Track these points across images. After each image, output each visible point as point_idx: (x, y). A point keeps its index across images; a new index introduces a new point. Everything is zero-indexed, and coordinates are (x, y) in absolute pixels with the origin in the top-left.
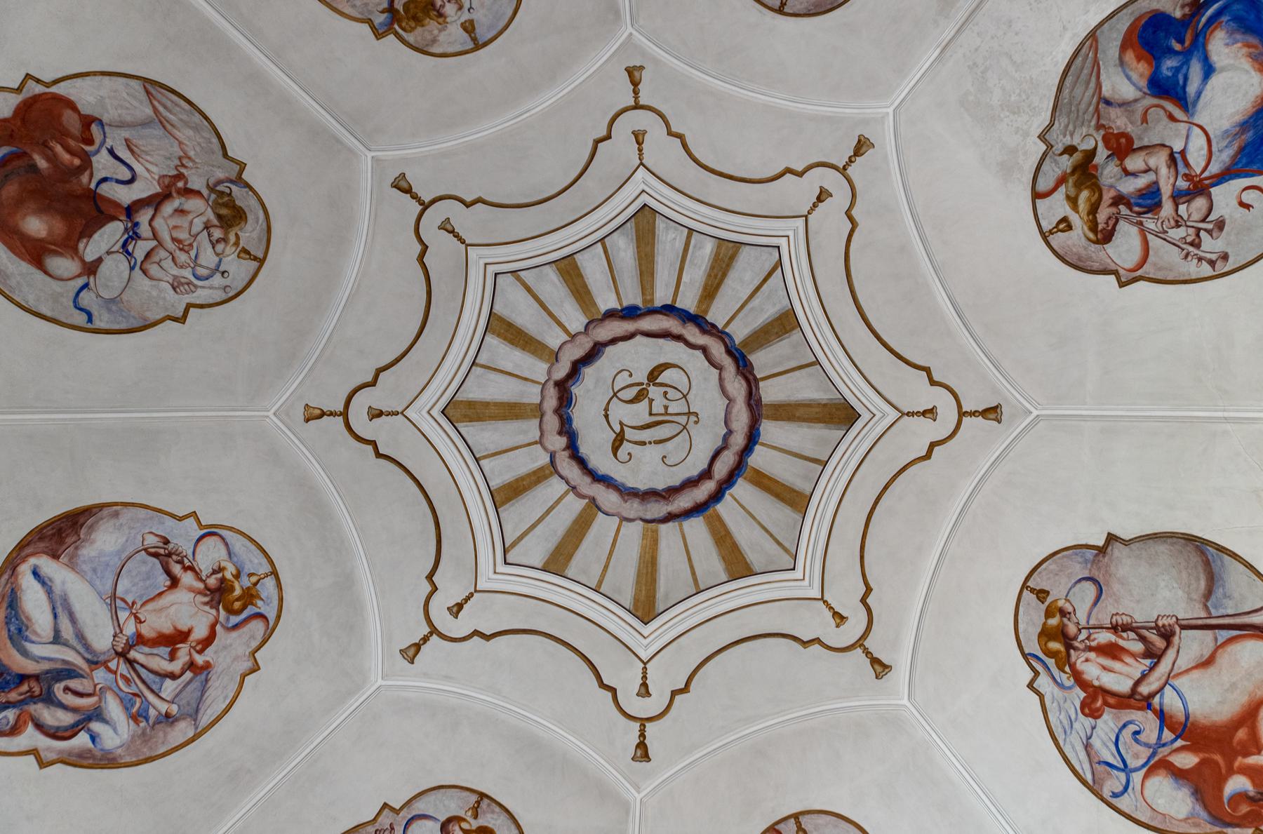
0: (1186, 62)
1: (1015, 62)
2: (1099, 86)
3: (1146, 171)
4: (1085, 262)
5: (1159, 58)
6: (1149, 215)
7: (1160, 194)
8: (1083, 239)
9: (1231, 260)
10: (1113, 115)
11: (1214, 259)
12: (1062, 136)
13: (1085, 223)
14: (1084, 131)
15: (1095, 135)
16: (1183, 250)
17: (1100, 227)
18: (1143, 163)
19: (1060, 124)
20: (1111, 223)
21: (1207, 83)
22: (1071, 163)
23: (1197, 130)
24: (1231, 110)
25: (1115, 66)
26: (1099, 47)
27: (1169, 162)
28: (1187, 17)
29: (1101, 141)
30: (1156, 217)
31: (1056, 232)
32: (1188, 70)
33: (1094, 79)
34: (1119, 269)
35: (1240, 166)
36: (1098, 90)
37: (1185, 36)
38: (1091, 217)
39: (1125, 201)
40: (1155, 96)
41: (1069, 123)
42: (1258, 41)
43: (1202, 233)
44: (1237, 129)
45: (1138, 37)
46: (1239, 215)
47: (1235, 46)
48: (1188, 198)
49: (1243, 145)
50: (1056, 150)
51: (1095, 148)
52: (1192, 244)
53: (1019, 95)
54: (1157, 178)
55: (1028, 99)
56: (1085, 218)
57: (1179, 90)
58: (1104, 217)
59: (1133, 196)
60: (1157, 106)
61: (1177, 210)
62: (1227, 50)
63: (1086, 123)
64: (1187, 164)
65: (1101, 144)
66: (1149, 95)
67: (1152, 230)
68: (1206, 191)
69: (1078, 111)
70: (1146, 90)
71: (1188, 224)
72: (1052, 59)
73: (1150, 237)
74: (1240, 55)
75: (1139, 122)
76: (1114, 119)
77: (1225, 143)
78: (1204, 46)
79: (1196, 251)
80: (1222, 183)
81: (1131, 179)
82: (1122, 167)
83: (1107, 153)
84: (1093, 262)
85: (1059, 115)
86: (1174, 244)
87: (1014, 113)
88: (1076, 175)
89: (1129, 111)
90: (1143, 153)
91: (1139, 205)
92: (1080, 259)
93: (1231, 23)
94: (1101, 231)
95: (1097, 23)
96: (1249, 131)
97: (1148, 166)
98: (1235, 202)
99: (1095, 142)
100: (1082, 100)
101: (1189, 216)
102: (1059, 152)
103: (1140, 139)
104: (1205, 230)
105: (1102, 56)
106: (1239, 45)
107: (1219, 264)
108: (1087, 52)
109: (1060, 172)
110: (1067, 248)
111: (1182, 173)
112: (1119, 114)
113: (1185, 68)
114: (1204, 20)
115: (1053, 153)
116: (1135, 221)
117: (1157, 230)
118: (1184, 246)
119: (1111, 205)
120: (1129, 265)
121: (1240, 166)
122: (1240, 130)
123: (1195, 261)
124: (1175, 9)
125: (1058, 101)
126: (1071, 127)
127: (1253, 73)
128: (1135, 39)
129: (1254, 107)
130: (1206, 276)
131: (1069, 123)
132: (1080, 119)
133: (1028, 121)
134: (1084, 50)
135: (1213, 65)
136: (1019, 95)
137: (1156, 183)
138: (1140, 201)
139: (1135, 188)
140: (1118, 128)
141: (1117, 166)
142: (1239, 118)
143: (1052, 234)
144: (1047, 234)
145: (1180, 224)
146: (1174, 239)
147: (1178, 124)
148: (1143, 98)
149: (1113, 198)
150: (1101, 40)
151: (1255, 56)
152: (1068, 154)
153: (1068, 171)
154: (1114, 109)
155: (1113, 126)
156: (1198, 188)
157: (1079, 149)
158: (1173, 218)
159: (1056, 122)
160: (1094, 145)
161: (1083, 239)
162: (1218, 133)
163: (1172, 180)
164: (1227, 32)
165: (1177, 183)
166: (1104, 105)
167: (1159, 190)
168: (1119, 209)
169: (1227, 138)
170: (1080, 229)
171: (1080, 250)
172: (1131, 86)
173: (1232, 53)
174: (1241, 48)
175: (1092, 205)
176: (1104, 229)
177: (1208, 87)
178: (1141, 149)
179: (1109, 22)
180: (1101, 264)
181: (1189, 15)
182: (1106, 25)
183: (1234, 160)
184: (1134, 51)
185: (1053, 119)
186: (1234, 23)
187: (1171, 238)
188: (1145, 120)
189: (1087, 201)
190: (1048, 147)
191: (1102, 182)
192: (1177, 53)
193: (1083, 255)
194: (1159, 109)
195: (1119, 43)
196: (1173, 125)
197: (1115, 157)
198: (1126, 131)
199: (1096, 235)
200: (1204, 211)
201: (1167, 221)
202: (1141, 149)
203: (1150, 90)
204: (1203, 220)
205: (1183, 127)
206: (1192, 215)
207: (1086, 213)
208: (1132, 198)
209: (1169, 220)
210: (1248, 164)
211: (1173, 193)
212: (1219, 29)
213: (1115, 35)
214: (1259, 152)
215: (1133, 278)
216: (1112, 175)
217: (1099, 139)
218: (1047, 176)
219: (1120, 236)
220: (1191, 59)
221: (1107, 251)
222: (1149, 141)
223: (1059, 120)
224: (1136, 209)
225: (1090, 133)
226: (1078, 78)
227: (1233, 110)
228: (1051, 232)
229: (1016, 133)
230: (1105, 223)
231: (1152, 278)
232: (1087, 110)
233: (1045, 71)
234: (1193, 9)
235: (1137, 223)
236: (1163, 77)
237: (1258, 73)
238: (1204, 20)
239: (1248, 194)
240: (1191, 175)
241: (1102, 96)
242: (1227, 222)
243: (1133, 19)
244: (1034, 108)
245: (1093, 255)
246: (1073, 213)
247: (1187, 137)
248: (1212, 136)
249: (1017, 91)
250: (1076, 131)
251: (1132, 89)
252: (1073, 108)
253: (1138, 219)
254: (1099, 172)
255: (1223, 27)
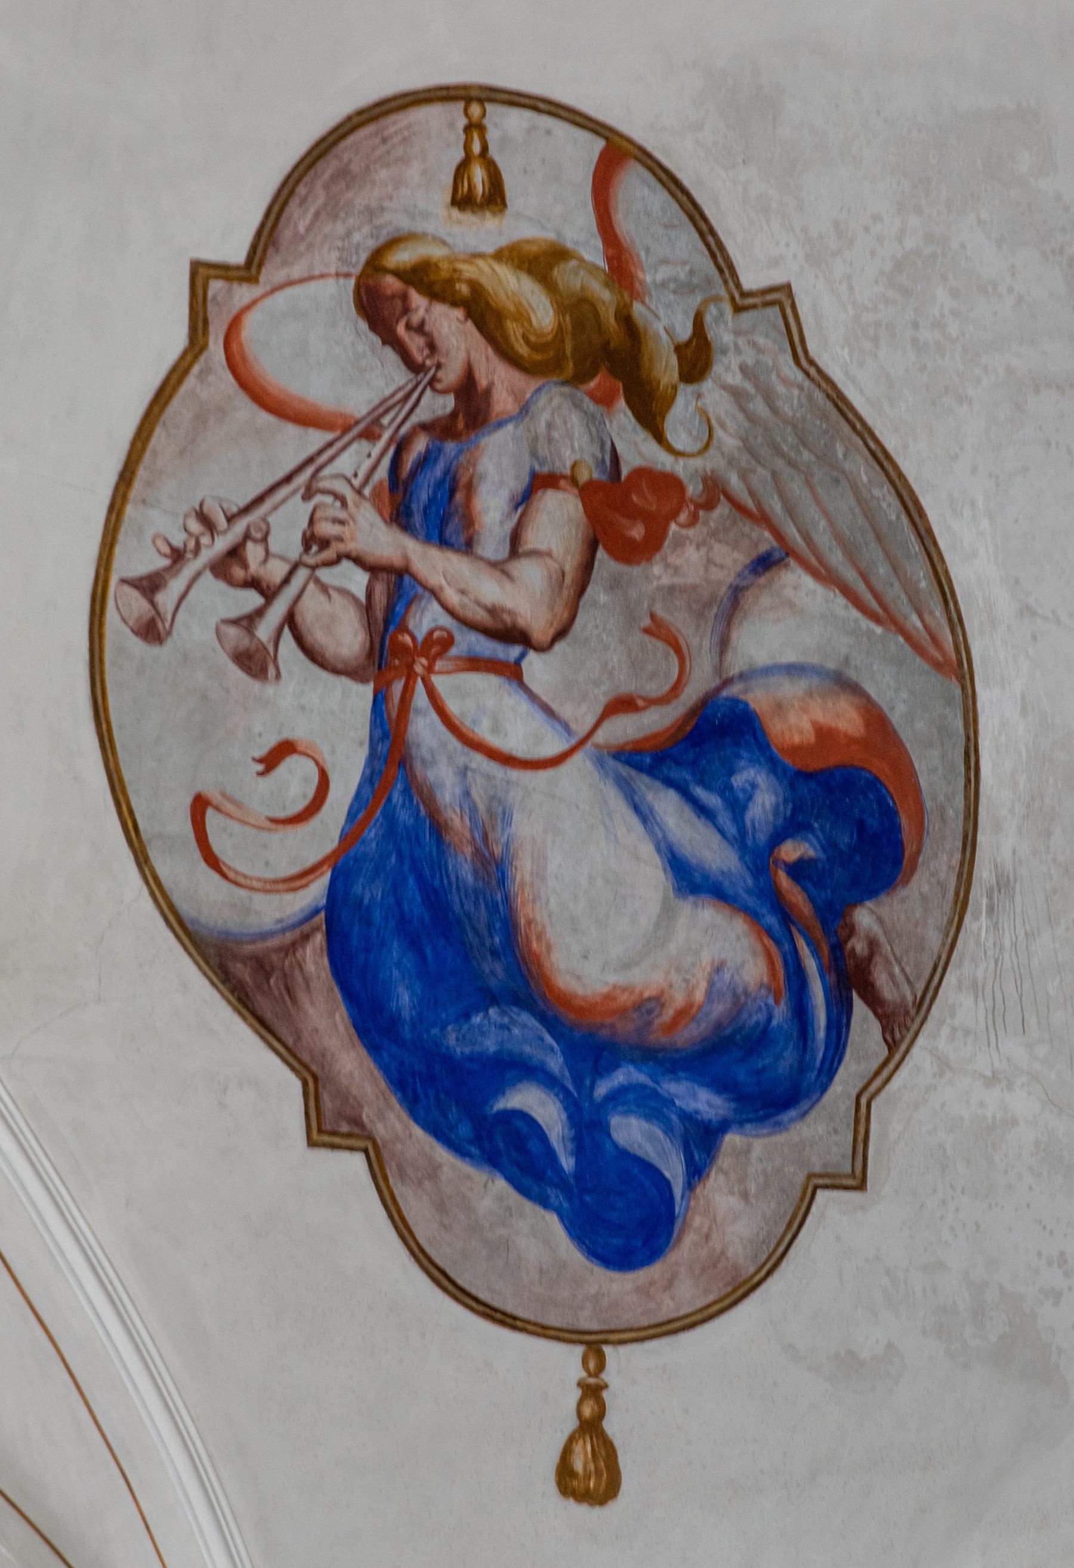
0: (740, 841)
1: (1037, 391)
2: (825, 575)
3: (515, 538)
4: (326, 187)
5: (792, 786)
6: (382, 472)
7: (428, 540)
8: (405, 224)
9: (136, 645)
10: (721, 552)
11: (160, 598)
12: (750, 362)
13: (452, 260)
14: (728, 441)
15: (697, 463)
16: (230, 519)
17: (418, 300)
18: (542, 547)
19: (785, 381)
20: (415, 344)
21: (659, 850)
22: (657, 335)
23: (552, 746)
24: (555, 861)
25: (847, 659)
26: (918, 659)
27: (507, 618)
28: (843, 933)
29: (668, 468)
30: (367, 491)
31: (467, 147)
32: (722, 833)
33: (850, 575)
34: (256, 291)
35: (397, 797)
36: (813, 561)
37: (805, 889)
38: (464, 289)
39: (461, 424)
40: (706, 702)
41: (775, 411)
42: (679, 1045)
43: (252, 599)
44: (497, 850)
45: (877, 778)
46: (257, 729)
47: (703, 985)
48: (379, 614)
49: (447, 839)
50: (721, 314)
51: (659, 437)
52: (235, 553)
53: (939, 325)
54: (481, 558)
55: (915, 341)
56: (468, 271)
57: (683, 774)
58: (445, 330)
59: (462, 459)
60: (676, 689)
61: (358, 561)
62: (706, 958)
63: (745, 459)
64: (475, 663)
65: (663, 461)
66: (718, 690)
67: (332, 459)
68: (373, 670)
69: (792, 464)
70: (734, 690)
71: (302, 574)
72: (973, 504)
73: (316, 438)
74: (675, 978)
75: (660, 613)
76: (711, 548)
77: (478, 795)
78: (752, 915)
79: (207, 555)
80: (374, 724)
81: (516, 484)
82: (564, 477)
83: (629, 464)
84: (317, 214)
85: (810, 398)
86: (259, 500)
87: (899, 266)
88: (612, 320)
89: (708, 605)
90: (571, 565)
91: (425, 461)
92: (344, 173)
93: (761, 1017)
94: (405, 297)
95: (979, 706)
96: (475, 872)
97: (534, 553)
98: (299, 732)
99: (678, 446)
100: (817, 501)
101: (324, 589)
102: (708, 319)
103: (615, 584)
104: (260, 613)
105: (893, 647)
106: (699, 996)
107: (137, 604)
108: (926, 616)
109: (648, 279)
110: (400, 151)
111: (458, 637)
112: (716, 574)
113: (732, 830)
114: (811, 965)
115: (716, 299)
116: (385, 421)
117: (326, 472)
118: (240, 527)
119: (469, 378)
120: (251, 329)
121: (397, 797)
122: (492, 854)
123: (178, 539)
124: (880, 920)
125: (853, 427)
126: (759, 407)
127: (613, 978)
128: (880, 768)
129: (529, 923)
130: (118, 550)
131: (775, 411)
132: (765, 452)
133: (851, 288)
134: (939, 612)
135: (691, 898)
136: (939, 325)
137: (468, 547)
138: (438, 470)
139: (482, 477)
140: (680, 543)
141: (574, 466)
142: (523, 869)
143: (468, 129)
144: (475, 110)
145: (315, 548)
146: (276, 508)
147: (599, 710)
148: (719, 669)
149: (488, 392)
150: (934, 681)
151: (649, 1012)
152: (688, 344)
153: (637, 309)
154: (739, 568)
155: (691, 532)
156: (394, 655)
157: (682, 386)
158: (340, 539)
159: (800, 376)
160: (670, 436)
161: (405, 224)
162: (514, 796)
163: (452, 597)
164: (746, 993)
165: (435, 606)
166: (763, 548)
167: (444, 543)
168: (444, 392)
169: (490, 811)
170: (442, 233)
171: (376, 193)
172: (769, 662)
173: (693, 965)
174: (690, 993)
175: (499, 316)
176: (406, 310)
177: (647, 849)
178: (587, 567)
179: (962, 741)
180: (298, 238)
181: (846, 941)
182: (960, 724)
183: (420, 793)
184: (852, 741)
185: (812, 371)
186: (757, 1023)
187: (284, 500)
188: (658, 630)
189: (519, 305)
190: (744, 294)
191: (556, 390)
192: (777, 838)
193: (350, 195)
194: (666, 688)
195: (896, 718)
196: (601, 697)
197: (604, 478)
198: (658, 557)
199: (397, 273)
200: (318, 636)
201: (342, 515)
202: (587, 567)
203: (727, 699)
204: (290, 620)
205: (582, 717)
206: (322, 598)
207: (484, 281)
208: (460, 452)
209: (342, 522)
210: (390, 819)
211: (413, 576)
212: (765, 980)
213: (920, 725)
214: (406, 867)
215: (206, 322)
216: (556, 435)
217: (680, 468)
218: (661, 231)
219: (360, 348)
220: (741, 858)
221: (331, 282)
222: (595, 603)
223: (801, 388)
224: (420, 445)
225: (712, 451)
226: (879, 537)
227: (552, 868)
228: (474, 127)
229: (836, 224)
230: (422, 323)
231: (180, 382)
232: (781, 496)
233: (956, 457)
234: (851, 963)
235: (377, 421)
236: (738, 756)
237: (605, 990)
238: (811, 965)
239: (306, 780)
240: (440, 655)
241: (792, 562)
242: (255, 686)
243: (928, 804)
244: (876, 340)
245: (340, 228)
246: (503, 241)
247: (549, 712)
248: (514, 774)
249: (953, 329)
250: (741, 416)
251: (761, 657)
252: (806, 456)
253: (386, 435)
254: (587, 400)
255: (763, 992)
